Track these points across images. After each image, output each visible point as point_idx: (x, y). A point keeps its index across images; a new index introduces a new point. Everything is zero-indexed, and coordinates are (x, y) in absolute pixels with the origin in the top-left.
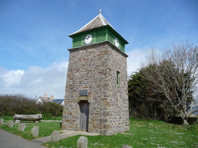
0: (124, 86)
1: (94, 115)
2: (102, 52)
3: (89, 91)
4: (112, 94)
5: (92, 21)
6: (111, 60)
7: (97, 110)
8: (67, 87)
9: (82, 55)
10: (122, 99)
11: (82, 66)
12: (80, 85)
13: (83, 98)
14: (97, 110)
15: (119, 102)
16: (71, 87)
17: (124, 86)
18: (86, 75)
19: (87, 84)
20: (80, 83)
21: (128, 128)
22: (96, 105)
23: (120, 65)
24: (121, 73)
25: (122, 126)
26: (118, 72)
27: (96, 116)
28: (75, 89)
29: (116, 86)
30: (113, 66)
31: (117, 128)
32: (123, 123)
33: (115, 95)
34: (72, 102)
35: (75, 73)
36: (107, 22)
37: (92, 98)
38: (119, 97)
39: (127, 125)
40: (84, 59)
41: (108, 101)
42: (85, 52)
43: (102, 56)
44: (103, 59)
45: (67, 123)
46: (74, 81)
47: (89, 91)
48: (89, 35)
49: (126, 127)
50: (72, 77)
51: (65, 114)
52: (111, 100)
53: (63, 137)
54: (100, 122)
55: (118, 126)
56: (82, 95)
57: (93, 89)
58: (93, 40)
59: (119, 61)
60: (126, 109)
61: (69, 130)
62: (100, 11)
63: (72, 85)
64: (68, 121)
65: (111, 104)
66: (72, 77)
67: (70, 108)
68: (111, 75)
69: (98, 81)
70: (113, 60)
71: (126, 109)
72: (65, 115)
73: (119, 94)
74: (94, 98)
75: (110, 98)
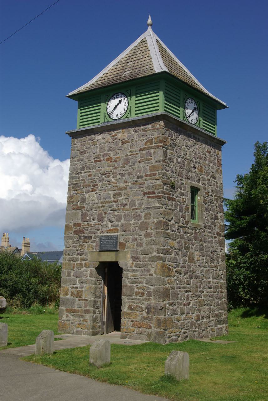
0: (213, 223)
1: (134, 297)
2: (150, 141)
4: (175, 245)
5: (128, 51)
6: (175, 160)
7: (139, 285)
8: (67, 228)
9: (102, 149)
10: (207, 255)
11: (104, 176)
12: (98, 224)
13: (108, 257)
14: (139, 285)
15: (197, 264)
16: (78, 228)
17: (213, 223)
18: (112, 199)
19: (117, 221)
20: (101, 219)
21: (224, 329)
22: (138, 273)
23: (201, 170)
24: (202, 192)
25: (205, 323)
26: (194, 191)
27: (139, 299)
28: (87, 233)
29: (190, 225)
30: (180, 174)
31: (192, 327)
32: (208, 317)
33: (187, 248)
34: (81, 266)
35: (87, 193)
37: (129, 256)
38: (197, 253)
39: (220, 322)
40: (108, 160)
41: (167, 262)
42: (111, 140)
43: (152, 151)
44: (153, 161)
45: (71, 317)
46: (84, 215)
47: (121, 240)
49: (219, 326)
50: (79, 203)
51: (67, 294)
52: (174, 260)
53: (63, 347)
54: (148, 313)
55: (193, 324)
56: (104, 249)
57: (130, 235)
58: (129, 110)
59: (198, 160)
60: (217, 283)
61: (77, 332)
62: (150, 21)
63: (79, 225)
64: (75, 311)
65: (175, 270)
66: (79, 203)
67: (78, 279)
68: (173, 200)
69: (143, 214)
70: (179, 160)
71: (217, 283)
72: (67, 299)
73: (197, 245)
74: (132, 257)
75: (173, 255)
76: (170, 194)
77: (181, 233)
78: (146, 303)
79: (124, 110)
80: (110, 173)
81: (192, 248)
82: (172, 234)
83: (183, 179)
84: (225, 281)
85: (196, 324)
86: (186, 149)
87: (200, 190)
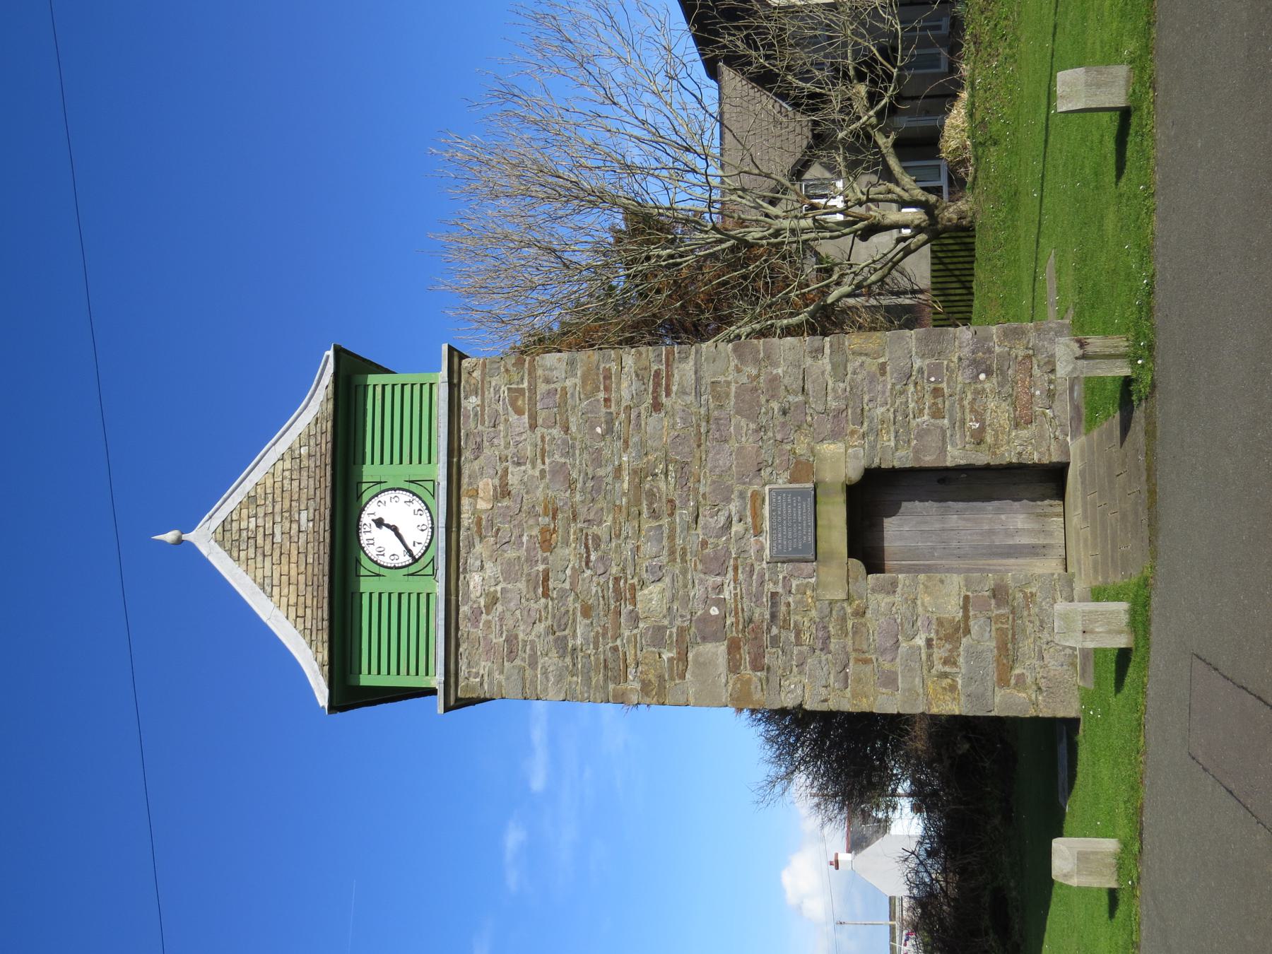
3: (782, 482)
12: (736, 569)
36: (322, 364)
43: (542, 388)
44: (568, 383)
48: (366, 519)
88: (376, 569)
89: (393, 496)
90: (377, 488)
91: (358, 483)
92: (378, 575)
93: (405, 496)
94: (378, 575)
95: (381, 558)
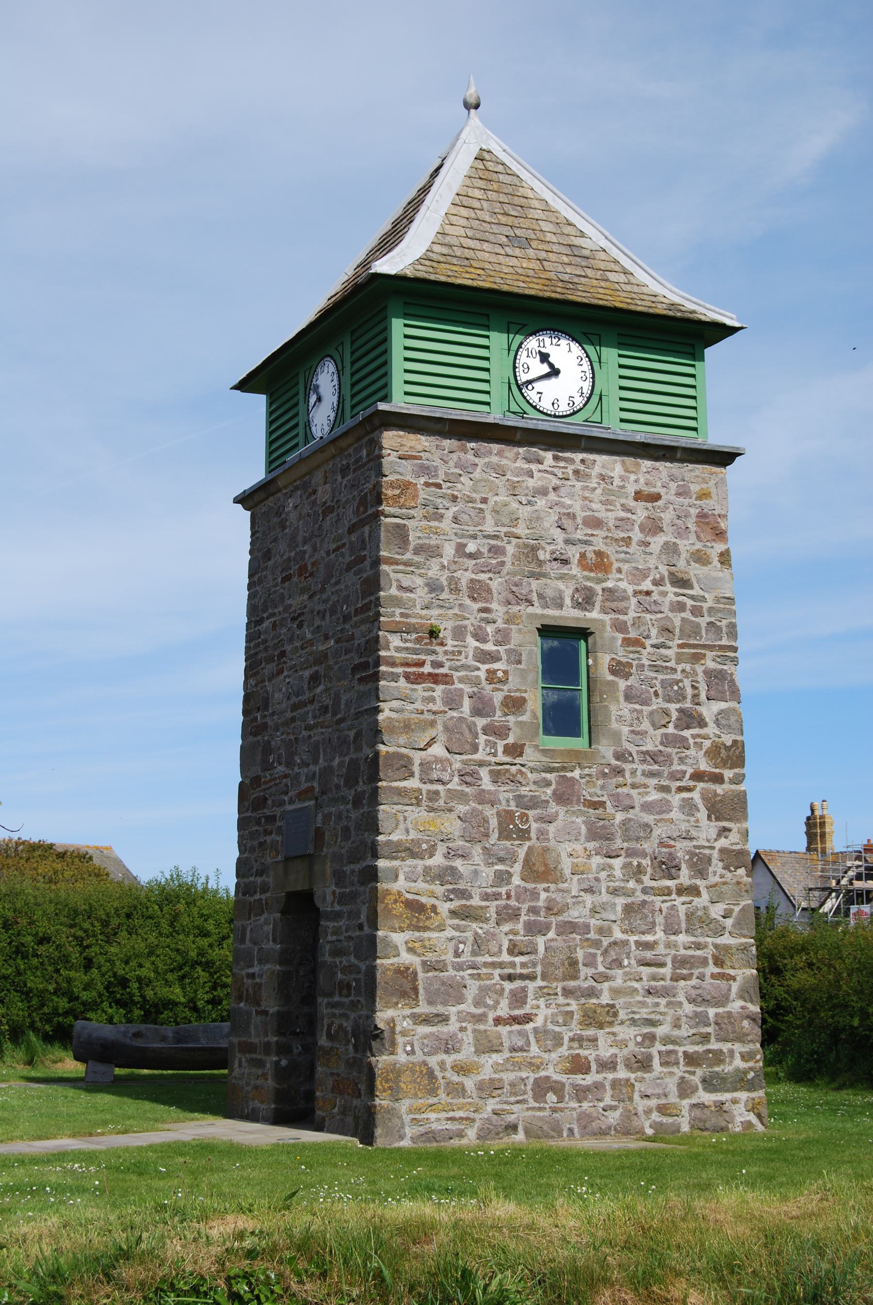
76: (421, 664)
77: (483, 787)
78: (353, 1016)
79: (582, 393)
80: (303, 614)
81: (542, 833)
82: (429, 792)
83: (494, 606)
84: (752, 940)
85: (567, 1087)
86: (515, 505)
87: (592, 633)
88: (514, 347)
89: (587, 374)
90: (594, 357)
91: (599, 335)
92: (509, 350)
93: (587, 387)
94: (509, 350)
95: (525, 353)
